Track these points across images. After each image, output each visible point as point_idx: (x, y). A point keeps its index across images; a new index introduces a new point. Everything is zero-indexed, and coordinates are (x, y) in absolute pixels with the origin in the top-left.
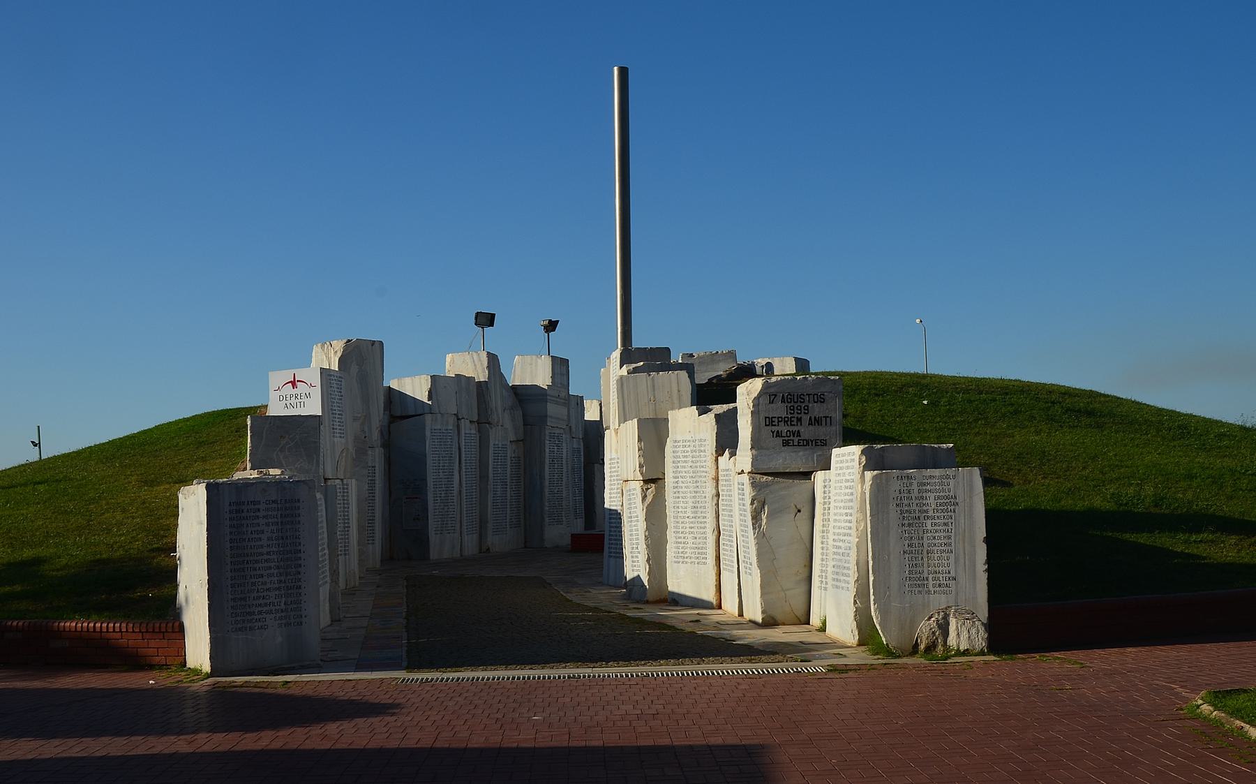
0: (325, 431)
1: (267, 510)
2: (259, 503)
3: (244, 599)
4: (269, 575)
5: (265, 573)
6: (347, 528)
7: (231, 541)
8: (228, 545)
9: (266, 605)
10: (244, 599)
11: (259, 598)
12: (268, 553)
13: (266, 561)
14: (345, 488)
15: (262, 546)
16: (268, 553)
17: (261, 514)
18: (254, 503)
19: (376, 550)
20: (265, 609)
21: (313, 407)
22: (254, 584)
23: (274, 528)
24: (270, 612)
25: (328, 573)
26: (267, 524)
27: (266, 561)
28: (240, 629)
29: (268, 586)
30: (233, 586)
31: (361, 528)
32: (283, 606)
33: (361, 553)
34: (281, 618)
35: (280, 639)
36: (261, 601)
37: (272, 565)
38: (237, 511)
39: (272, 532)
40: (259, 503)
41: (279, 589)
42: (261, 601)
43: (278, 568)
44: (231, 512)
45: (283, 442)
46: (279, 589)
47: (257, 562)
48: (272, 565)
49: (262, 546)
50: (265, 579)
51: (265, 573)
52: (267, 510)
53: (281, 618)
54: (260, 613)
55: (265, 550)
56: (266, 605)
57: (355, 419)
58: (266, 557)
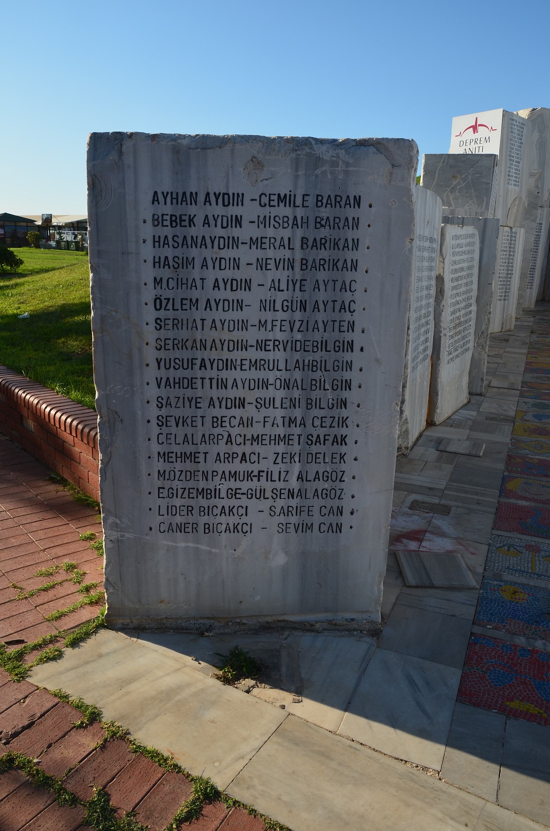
0: (499, 173)
1: (264, 222)
2: (239, 199)
3: (193, 457)
4: (261, 404)
5: (251, 396)
6: (509, 274)
7: (159, 303)
8: (150, 314)
9: (249, 476)
10: (193, 457)
11: (230, 457)
12: (262, 345)
13: (255, 364)
14: (513, 236)
15: (244, 325)
16: (262, 345)
17: (246, 232)
18: (227, 199)
19: (533, 293)
20: (245, 486)
21: (493, 147)
22: (218, 421)
23: (283, 275)
24: (262, 494)
25: (472, 338)
26: (263, 265)
27: (255, 364)
28: (182, 528)
29: (257, 429)
30: (162, 422)
31: (523, 277)
32: (294, 484)
33: (520, 296)
34: (286, 511)
35: (280, 559)
36: (236, 466)
37: (271, 376)
38: (176, 221)
39: (275, 286)
40: (239, 199)
41: (286, 439)
42: (236, 466)
43: (287, 385)
44: (157, 221)
45: (454, 183)
46: (286, 439)
47: (229, 365)
48: (271, 376)
49: (244, 325)
50: (250, 411)
51: (251, 396)
52: (264, 222)
53: (286, 511)
54: (234, 493)
55: (252, 335)
56: (249, 476)
57: (532, 175)
58: (253, 354)
